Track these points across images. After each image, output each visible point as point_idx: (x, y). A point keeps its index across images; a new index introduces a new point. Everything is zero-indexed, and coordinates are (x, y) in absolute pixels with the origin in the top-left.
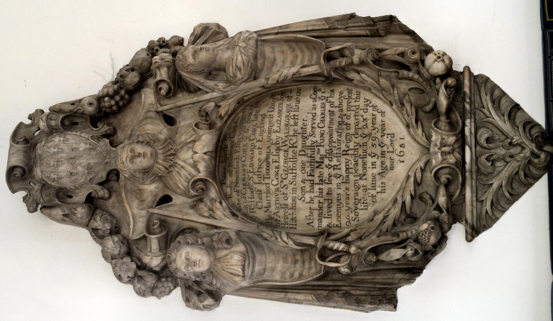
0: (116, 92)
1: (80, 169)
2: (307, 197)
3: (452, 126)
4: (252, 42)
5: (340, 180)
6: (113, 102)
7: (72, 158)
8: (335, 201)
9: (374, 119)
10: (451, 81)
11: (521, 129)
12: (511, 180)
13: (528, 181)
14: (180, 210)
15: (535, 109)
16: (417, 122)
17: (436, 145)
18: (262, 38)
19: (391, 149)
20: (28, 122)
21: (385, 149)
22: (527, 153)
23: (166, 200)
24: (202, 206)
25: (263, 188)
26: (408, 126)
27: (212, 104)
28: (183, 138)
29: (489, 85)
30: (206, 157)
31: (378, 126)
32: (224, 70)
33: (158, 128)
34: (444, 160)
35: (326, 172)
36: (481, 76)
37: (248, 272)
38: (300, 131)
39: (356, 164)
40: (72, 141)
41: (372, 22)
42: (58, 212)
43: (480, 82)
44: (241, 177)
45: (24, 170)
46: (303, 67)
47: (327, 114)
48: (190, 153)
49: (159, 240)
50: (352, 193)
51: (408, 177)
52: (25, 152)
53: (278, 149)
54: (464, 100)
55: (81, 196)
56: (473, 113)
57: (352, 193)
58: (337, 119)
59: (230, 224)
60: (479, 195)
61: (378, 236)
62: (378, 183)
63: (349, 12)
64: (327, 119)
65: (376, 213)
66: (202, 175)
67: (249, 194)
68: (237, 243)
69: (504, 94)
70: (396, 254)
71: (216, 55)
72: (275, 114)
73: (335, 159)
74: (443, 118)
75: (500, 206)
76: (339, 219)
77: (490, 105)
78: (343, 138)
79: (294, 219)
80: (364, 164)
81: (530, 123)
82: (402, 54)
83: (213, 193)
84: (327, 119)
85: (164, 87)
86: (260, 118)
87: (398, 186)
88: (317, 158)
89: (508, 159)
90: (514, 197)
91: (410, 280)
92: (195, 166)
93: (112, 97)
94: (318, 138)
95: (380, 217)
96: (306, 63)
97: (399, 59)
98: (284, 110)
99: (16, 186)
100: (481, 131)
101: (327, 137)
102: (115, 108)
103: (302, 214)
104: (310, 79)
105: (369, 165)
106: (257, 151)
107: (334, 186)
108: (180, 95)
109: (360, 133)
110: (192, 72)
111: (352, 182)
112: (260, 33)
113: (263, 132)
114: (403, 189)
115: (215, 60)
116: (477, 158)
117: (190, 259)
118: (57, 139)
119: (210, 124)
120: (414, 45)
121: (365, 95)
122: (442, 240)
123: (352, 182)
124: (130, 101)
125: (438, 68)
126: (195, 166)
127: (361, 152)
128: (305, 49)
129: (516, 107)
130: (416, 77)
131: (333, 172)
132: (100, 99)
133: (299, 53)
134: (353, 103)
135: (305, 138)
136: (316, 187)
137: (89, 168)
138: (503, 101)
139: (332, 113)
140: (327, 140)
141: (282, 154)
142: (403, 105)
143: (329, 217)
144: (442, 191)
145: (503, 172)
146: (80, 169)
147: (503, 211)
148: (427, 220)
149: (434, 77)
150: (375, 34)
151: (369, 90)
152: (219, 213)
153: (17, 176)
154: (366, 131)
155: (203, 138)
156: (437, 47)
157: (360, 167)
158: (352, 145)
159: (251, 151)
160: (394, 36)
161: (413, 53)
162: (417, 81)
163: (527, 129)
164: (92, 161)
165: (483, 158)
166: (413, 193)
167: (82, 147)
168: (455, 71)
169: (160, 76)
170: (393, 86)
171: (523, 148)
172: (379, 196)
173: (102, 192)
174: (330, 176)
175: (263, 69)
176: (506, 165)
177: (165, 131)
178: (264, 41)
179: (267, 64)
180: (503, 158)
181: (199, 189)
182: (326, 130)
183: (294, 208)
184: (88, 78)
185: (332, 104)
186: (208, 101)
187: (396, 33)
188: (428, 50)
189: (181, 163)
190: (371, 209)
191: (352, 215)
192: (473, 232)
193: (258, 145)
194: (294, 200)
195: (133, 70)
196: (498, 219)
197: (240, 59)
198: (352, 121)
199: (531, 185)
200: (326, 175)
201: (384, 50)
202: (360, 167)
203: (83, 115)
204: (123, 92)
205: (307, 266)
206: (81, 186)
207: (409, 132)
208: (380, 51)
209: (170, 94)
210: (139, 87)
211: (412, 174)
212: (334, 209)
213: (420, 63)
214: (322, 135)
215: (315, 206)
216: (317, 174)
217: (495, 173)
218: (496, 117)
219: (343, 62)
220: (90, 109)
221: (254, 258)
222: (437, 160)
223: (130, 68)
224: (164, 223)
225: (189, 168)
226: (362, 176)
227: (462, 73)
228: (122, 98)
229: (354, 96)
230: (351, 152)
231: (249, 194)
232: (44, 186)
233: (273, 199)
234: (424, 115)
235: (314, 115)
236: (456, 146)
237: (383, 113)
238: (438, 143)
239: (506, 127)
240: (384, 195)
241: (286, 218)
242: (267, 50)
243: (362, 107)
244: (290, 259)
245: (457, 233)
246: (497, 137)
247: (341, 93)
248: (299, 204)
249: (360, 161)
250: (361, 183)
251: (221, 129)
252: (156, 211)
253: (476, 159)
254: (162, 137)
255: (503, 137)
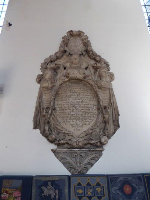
0: (94, 54)
1: (73, 48)
2: (65, 104)
3: (86, 144)
4: (109, 87)
5: (69, 112)
6: (91, 54)
7: (77, 46)
8: (63, 111)
9: (87, 122)
10: (99, 144)
11: (85, 166)
12: (68, 163)
13: (69, 168)
14: (62, 72)
15: (92, 171)
16: (87, 134)
17: (79, 140)
18: (110, 90)
19: (78, 126)
20: (85, 35)
21: (78, 125)
22: (78, 168)
23: (65, 68)
24: (63, 77)
25: (67, 92)
26: (85, 131)
27: (91, 78)
28: (81, 71)
29: (99, 156)
30: (75, 76)
31: (85, 123)
32: (100, 80)
33: (84, 65)
34: (74, 142)
35: (71, 108)
36: (102, 154)
37: (44, 89)
38: (83, 101)
39: (74, 117)
40: (80, 45)
41: (117, 120)
42: (62, 44)
43: (100, 154)
44: (70, 86)
45: (72, 34)
46: (102, 101)
47: (89, 108)
48: (76, 73)
49: (54, 67)
50: (66, 116)
51: (70, 132)
52: (77, 34)
53: (78, 95)
54: (94, 148)
55: (66, 49)
56: (90, 151)
57: (66, 116)
58: (87, 111)
59: (58, 84)
60: (65, 153)
61: (53, 123)
62: (68, 123)
63: (120, 114)
64: (87, 108)
65: (59, 123)
66: (71, 76)
67: (66, 88)
68: (51, 85)
69: (96, 161)
70: (47, 128)
71: (104, 77)
72: (89, 94)
73: (75, 111)
74: (87, 142)
75: (61, 159)
76: (58, 112)
77: (93, 157)
78: (81, 113)
79: (59, 101)
80: (74, 119)
81: (87, 169)
82: (107, 129)
83: (66, 80)
84: (87, 108)
85: (95, 65)
86: (87, 90)
87: (67, 129)
88: (75, 106)
89: (75, 162)
90: (64, 164)
91: (41, 133)
92: (73, 74)
93: (92, 54)
94: (81, 106)
95: (58, 124)
96: (103, 102)
97: (106, 129)
98: (90, 97)
99: (68, 33)
100: (84, 154)
101: (82, 108)
102: (90, 55)
103: (60, 103)
104: (99, 103)
105: (73, 120)
106: (77, 89)
107: (68, 111)
108: (93, 70)
109: (83, 118)
110: (99, 71)
111: (69, 116)
112: (112, 89)
113: (83, 91)
114: (66, 130)
115: (102, 77)
116: (76, 152)
117: (49, 74)
118: (81, 42)
119: (85, 77)
120: (111, 133)
121: (95, 119)
122: (52, 142)
123: (69, 116)
124: (92, 59)
125: (103, 140)
126: (73, 74)
127: (77, 118)
128: (108, 102)
129: (92, 165)
130: (101, 134)
131: (72, 110)
132: (92, 51)
133: (106, 101)
134: (92, 116)
135: (81, 102)
136: (67, 106)
137: (73, 50)
138: (94, 161)
139: (89, 110)
140: (80, 108)
141: (77, 96)
142: (92, 130)
143: (59, 110)
144: (65, 142)
145: (71, 161)
146: (73, 48)
147: (60, 161)
148: (56, 136)
149: (100, 139)
150: (113, 122)
151: (96, 120)
152: (61, 81)
153: (71, 33)
154: (83, 119)
155: (81, 75)
156: (110, 141)
157: (73, 118)
158: (79, 115)
159: (77, 88)
160: (113, 127)
161: (107, 132)
162: (99, 134)
163: (85, 168)
164: (75, 51)
165: (76, 154)
166: (65, 133)
167: (79, 48)
168: (103, 146)
169: (99, 65)
170: (97, 127)
171: (79, 167)
172: (64, 123)
173: (67, 54)
174: (70, 110)
175: (101, 90)
176: (74, 161)
177: (84, 67)
178: (110, 90)
179: (103, 91)
180: (76, 161)
181: (67, 76)
182: (84, 108)
183: (62, 100)
184: (97, 48)
185: (92, 110)
186: (92, 77)
187: (114, 128)
188: (109, 137)
189: (74, 71)
190: (61, 121)
191: (59, 116)
192: (54, 151)
193: (79, 90)
194: (64, 100)
195: (100, 58)
196: (58, 158)
197: (103, 83)
198: (87, 115)
199: (68, 169)
200: (70, 108)
201: (109, 124)
202: (73, 118)
203: (87, 47)
204: (94, 56)
205: (46, 104)
206: (69, 49)
207: (84, 132)
208: (108, 122)
209: (93, 67)
210: (96, 61)
211: (63, 129)
212: (61, 111)
213: (104, 135)
214: (82, 107)
215: (62, 106)
216: (71, 106)
217: (72, 158)
218: (88, 159)
219: (104, 112)
220: (89, 49)
221: (48, 90)
222: (74, 140)
223: (100, 58)
224: (58, 68)
225: (72, 73)
226: (70, 118)
227: (103, 148)
228: (92, 56)
229: (94, 116)
230: (77, 115)
231: (66, 88)
232: (68, 40)
233: (64, 94)
234: (88, 135)
235: (88, 105)
236: (79, 146)
237: (89, 124)
238: (79, 140)
239: (86, 162)
240: (65, 125)
241: (59, 98)
242: (108, 92)
243: (91, 118)
244: (48, 100)
245: (54, 147)
246: (83, 159)
247: (95, 112)
248: (63, 102)
249: (75, 118)
250: (68, 118)
251: (84, 81)
252: (62, 66)
253: (76, 152)
254: (82, 67)
255: (83, 161)
